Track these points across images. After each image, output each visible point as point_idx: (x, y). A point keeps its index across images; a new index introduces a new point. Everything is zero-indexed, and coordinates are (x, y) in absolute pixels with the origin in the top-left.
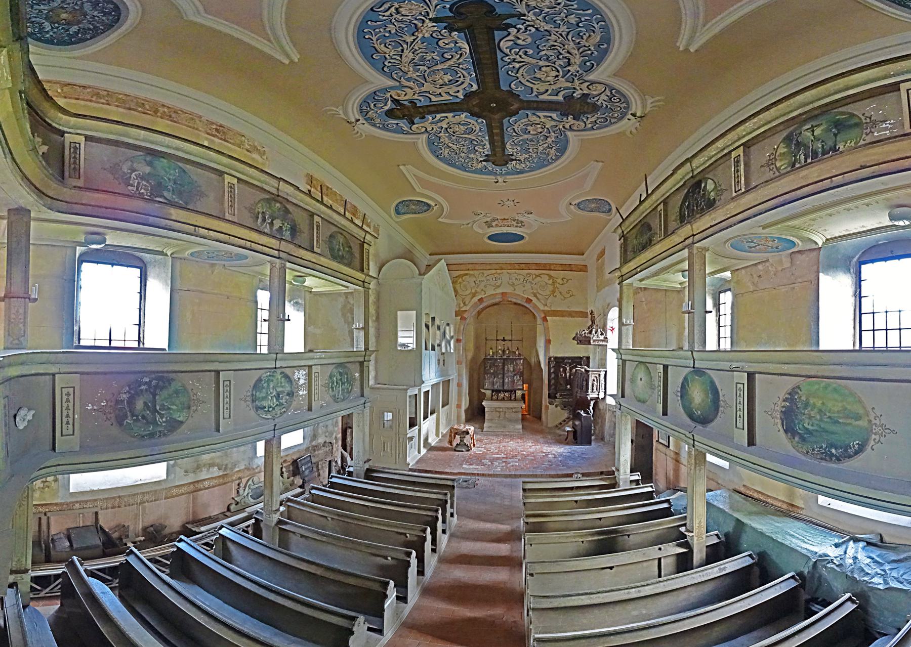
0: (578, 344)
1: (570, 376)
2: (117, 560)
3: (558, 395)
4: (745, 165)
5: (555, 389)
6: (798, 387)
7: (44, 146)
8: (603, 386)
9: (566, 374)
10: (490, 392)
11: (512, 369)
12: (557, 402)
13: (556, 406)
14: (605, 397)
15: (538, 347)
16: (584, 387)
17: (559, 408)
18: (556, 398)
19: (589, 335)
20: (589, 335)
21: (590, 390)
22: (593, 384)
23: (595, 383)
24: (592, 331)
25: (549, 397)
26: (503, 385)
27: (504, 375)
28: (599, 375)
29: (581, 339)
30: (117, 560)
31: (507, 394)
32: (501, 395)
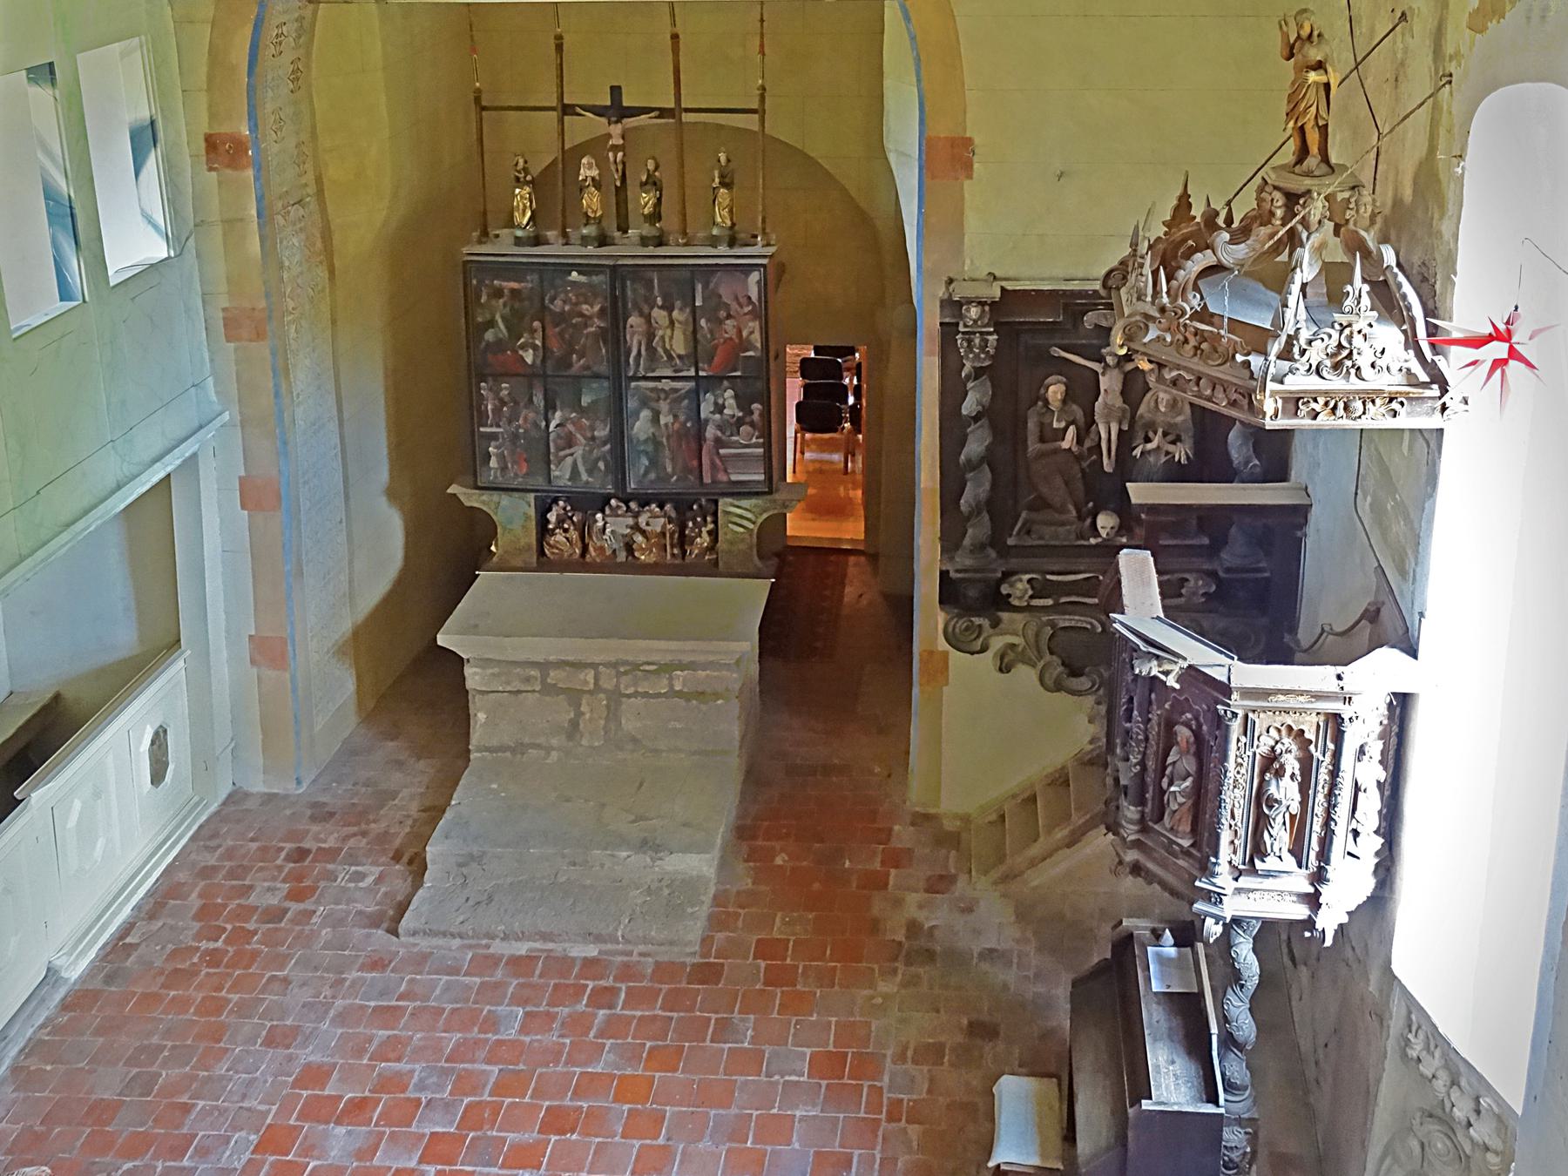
3: (1019, 589)
5: (996, 541)
8: (1371, 804)
9: (1087, 426)
10: (526, 507)
11: (679, 346)
12: (1013, 630)
13: (1004, 668)
17: (1025, 675)
18: (1003, 603)
21: (1227, 854)
22: (1261, 802)
23: (1286, 791)
25: (949, 592)
26: (619, 465)
27: (618, 380)
28: (1335, 724)
31: (655, 521)
32: (612, 526)
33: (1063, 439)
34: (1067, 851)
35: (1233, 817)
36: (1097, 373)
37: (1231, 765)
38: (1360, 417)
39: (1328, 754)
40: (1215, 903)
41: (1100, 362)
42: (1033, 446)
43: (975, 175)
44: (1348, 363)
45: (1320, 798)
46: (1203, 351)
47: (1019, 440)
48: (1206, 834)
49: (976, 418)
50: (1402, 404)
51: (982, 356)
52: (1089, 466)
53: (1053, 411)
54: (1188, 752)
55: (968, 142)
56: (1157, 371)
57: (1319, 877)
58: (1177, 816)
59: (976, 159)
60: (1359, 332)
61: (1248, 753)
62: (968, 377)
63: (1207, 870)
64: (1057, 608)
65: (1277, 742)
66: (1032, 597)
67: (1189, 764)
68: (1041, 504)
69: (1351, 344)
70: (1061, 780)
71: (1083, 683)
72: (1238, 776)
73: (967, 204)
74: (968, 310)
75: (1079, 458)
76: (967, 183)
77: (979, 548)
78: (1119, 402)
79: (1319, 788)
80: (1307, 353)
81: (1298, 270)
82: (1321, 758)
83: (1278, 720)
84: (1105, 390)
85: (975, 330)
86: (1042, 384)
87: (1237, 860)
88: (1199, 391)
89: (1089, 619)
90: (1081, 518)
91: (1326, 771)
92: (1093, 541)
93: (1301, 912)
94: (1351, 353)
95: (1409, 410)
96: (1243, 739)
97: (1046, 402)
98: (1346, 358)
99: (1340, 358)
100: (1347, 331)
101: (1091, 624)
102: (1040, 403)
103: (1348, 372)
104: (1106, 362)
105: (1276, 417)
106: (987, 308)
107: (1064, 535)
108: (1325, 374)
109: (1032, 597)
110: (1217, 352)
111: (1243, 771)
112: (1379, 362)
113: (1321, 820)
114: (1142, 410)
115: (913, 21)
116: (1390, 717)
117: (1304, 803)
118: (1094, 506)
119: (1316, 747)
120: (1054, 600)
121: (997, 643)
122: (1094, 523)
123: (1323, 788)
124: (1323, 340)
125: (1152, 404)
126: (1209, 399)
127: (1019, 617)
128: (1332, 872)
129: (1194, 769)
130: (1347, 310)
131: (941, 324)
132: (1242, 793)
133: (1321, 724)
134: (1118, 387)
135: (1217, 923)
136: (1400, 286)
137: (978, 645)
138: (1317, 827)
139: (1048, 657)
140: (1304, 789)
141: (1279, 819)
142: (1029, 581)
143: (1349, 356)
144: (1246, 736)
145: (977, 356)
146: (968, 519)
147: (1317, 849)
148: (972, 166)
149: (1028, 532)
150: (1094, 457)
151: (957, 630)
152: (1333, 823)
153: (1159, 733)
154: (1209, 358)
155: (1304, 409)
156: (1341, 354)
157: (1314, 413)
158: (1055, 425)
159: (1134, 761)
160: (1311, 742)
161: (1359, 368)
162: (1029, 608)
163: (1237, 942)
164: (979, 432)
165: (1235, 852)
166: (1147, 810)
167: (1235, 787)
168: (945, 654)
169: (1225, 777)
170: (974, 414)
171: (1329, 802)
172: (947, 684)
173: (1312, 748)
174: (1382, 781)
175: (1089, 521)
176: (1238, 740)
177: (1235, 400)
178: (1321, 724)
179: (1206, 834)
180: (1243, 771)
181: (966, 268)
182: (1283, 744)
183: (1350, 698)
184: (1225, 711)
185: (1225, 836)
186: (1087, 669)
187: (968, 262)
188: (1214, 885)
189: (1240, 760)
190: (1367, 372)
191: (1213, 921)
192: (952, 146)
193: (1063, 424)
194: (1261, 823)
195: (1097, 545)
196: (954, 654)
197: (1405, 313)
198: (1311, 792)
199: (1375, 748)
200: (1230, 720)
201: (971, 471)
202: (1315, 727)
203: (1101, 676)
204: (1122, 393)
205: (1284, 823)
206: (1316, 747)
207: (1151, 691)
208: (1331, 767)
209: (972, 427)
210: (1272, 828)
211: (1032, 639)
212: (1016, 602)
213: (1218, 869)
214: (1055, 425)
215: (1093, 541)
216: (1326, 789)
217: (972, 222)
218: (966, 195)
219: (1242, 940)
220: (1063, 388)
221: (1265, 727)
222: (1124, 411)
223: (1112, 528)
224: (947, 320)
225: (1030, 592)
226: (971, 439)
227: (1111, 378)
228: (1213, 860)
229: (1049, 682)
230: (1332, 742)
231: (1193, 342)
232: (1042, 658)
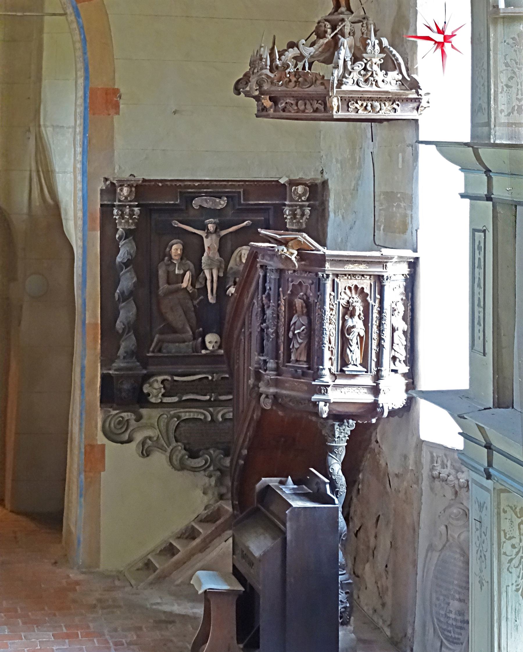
0: (262, 111)
1: (222, 283)
2: (259, 506)
4: (494, 84)
6: (467, 491)
7: (353, 634)
8: (400, 340)
9: (199, 270)
13: (145, 453)
14: (410, 403)
15: (48, 132)
16: (298, 344)
19: (319, 68)
20: (319, 68)
24: (335, 45)
28: (379, 279)
29: (279, 89)
30: (259, 506)
33: (182, 282)
34: (200, 554)
35: (330, 343)
36: (201, 237)
37: (327, 307)
38: (379, 112)
39: (377, 301)
40: (324, 394)
41: (204, 230)
42: (163, 287)
43: (121, 112)
44: (372, 79)
45: (375, 329)
46: (299, 82)
47: (153, 276)
48: (316, 358)
49: (126, 264)
50: (398, 105)
51: (131, 221)
52: (198, 304)
53: (175, 264)
54: (303, 314)
55: (116, 92)
56: (274, 107)
57: (378, 377)
58: (299, 351)
59: (121, 102)
60: (375, 64)
61: (336, 302)
62: (120, 238)
63: (318, 375)
64: (180, 404)
65: (350, 298)
66: (164, 395)
67: (304, 320)
68: (171, 329)
69: (372, 69)
70: (187, 534)
71: (199, 462)
72: (331, 316)
73: (116, 130)
74: (121, 190)
75: (192, 297)
76: (116, 117)
77: (130, 354)
78: (217, 257)
79: (374, 322)
80: (352, 74)
81: (342, 47)
82: (374, 304)
83: (353, 282)
84: (209, 247)
85: (127, 204)
86: (168, 245)
87: (334, 369)
88: (298, 108)
89: (202, 411)
90: (195, 338)
91: (377, 312)
92: (203, 352)
93: (369, 398)
94: (372, 74)
95: (402, 109)
96: (333, 293)
97: (171, 258)
98: (370, 76)
99: (367, 77)
100: (370, 63)
101: (204, 414)
102: (166, 258)
103: (372, 84)
104: (208, 229)
105: (338, 111)
106: (133, 189)
107: (185, 348)
108: (361, 85)
109: (164, 395)
110: (307, 82)
111: (334, 313)
112: (386, 79)
113: (376, 342)
114: (231, 264)
115: (82, 14)
116: (407, 296)
117: (366, 332)
118: (203, 330)
119: (371, 298)
120: (179, 397)
121: (139, 437)
122: (203, 342)
123: (376, 322)
124: (359, 67)
125: (238, 259)
126: (304, 111)
127: (155, 413)
128: (383, 384)
129: (307, 322)
130: (369, 52)
131: (102, 205)
132: (334, 327)
133: (372, 284)
134: (216, 246)
135: (325, 405)
136: (391, 52)
137: (126, 437)
138: (375, 343)
139: (174, 444)
140: (366, 323)
141: (355, 341)
142: (163, 382)
143: (372, 75)
144: (334, 292)
145: (127, 222)
146: (121, 335)
147: (375, 360)
148: (119, 106)
149: (160, 351)
150: (202, 297)
151: (112, 425)
152: (383, 341)
153: (285, 311)
154: (303, 85)
155: (352, 107)
156: (367, 74)
157: (357, 110)
158: (177, 272)
159: (272, 331)
160: (367, 295)
161: (377, 82)
162: (161, 404)
163: (332, 463)
164: (128, 274)
165: (332, 365)
166: (280, 362)
167: (330, 323)
168: (103, 446)
169: (325, 315)
170: (125, 261)
171: (380, 330)
172: (104, 470)
173: (368, 298)
174: (406, 330)
175: (200, 339)
176: (330, 294)
177: (317, 108)
178: (372, 284)
179: (316, 358)
180: (334, 313)
181: (116, 171)
182: (353, 298)
183: (386, 265)
184: (323, 275)
185: (327, 354)
186: (201, 453)
187: (117, 167)
188: (323, 382)
189: (331, 307)
190: (380, 83)
191: (323, 403)
192: (106, 94)
193: (182, 272)
194: (345, 343)
195: (205, 355)
196: (110, 446)
197: (395, 62)
198: (370, 325)
199: (401, 308)
200: (325, 280)
201: (123, 302)
202: (369, 286)
203: (210, 455)
204: (219, 251)
205: (357, 343)
206: (371, 298)
207: (279, 287)
208: (379, 309)
209: (124, 271)
210: (351, 346)
211: (163, 429)
212: (153, 400)
213: (324, 372)
214: (177, 272)
215: (203, 352)
216: (378, 322)
217: (119, 142)
218: (115, 124)
219: (335, 461)
220: (181, 246)
221: (343, 288)
222: (220, 262)
223: (216, 342)
224: (106, 202)
225: (163, 391)
226: (122, 279)
227: (212, 239)
228: (321, 367)
229: (176, 463)
230: (378, 294)
231: (294, 79)
232: (170, 445)
